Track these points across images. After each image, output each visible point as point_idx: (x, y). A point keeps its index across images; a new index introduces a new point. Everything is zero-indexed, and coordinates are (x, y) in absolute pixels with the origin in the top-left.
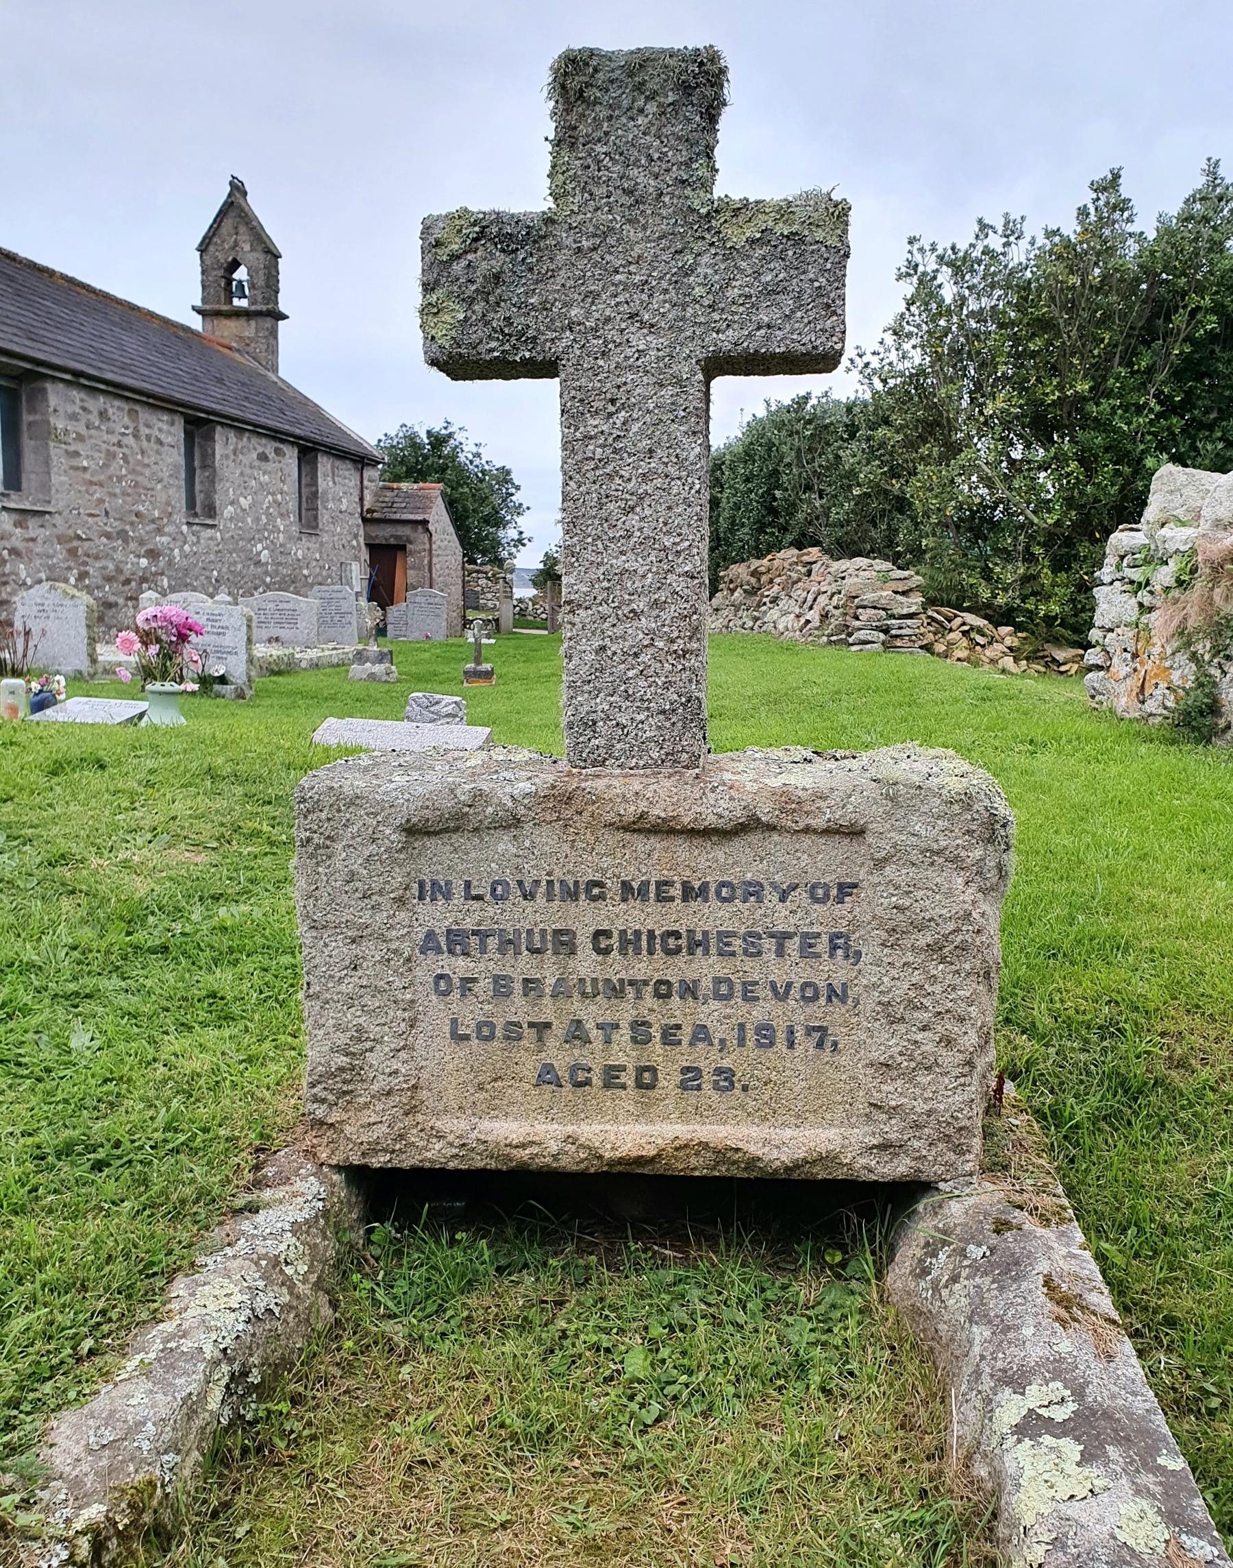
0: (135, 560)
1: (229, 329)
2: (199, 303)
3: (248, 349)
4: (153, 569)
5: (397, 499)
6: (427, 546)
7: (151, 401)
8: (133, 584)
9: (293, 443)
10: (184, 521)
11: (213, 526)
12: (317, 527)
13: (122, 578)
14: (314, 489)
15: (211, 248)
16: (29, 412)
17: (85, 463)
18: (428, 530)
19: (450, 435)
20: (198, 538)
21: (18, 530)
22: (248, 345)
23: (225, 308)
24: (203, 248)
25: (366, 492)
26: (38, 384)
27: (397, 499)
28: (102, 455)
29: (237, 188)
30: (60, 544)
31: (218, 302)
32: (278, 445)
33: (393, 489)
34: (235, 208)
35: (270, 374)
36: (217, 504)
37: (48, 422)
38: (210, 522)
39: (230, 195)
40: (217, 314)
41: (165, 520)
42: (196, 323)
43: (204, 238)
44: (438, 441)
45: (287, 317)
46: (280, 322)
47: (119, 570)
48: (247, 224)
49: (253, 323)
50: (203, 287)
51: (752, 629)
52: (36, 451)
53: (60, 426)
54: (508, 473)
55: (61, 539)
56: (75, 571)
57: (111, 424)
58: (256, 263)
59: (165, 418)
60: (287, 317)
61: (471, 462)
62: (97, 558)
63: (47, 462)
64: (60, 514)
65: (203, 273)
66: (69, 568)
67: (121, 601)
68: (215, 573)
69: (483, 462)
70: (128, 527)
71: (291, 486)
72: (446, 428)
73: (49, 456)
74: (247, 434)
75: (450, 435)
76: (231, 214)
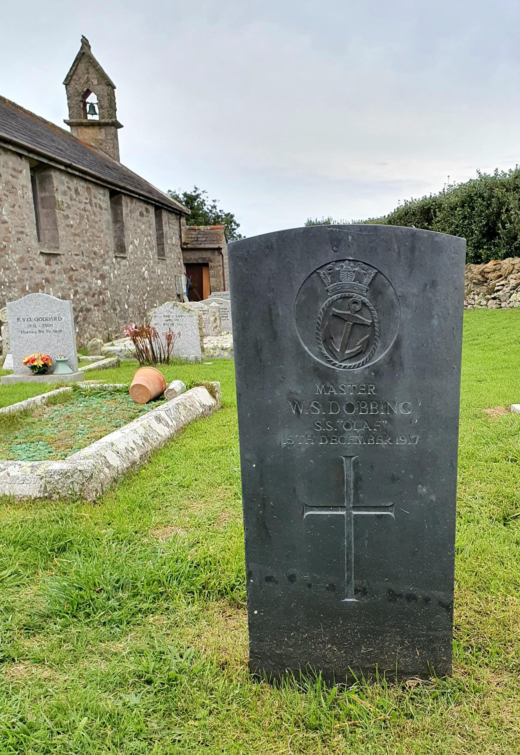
0: (96, 281)
1: (87, 135)
2: (67, 118)
3: (101, 147)
4: (103, 286)
5: (199, 236)
6: (221, 263)
7: (98, 181)
8: (96, 296)
9: (152, 204)
10: (114, 255)
11: (125, 258)
12: (164, 255)
13: (91, 293)
14: (161, 232)
15: (72, 82)
16: (42, 192)
17: (72, 223)
18: (221, 253)
19: (198, 196)
20: (120, 265)
21: (47, 267)
22: (101, 144)
23: (85, 121)
24: (67, 82)
25: (182, 232)
26: (48, 173)
27: (199, 236)
28: (78, 217)
29: (85, 42)
30: (65, 274)
31: (80, 117)
32: (146, 206)
33: (195, 230)
34: (85, 56)
35: (117, 162)
36: (126, 244)
37: (54, 197)
38: (122, 255)
39: (82, 48)
40: (80, 125)
41: (106, 256)
42: (67, 128)
43: (68, 76)
44: (190, 199)
45: (122, 126)
46: (118, 130)
47: (90, 288)
48: (94, 67)
49: (103, 130)
50: (69, 107)
51: (486, 305)
52: (47, 215)
53: (60, 200)
54: (232, 216)
55: (66, 271)
56: (72, 290)
57: (80, 197)
58: (102, 92)
59: (102, 192)
60: (122, 126)
61: (211, 211)
62: (81, 281)
63: (55, 223)
64: (64, 255)
65: (68, 98)
66: (70, 289)
67: (92, 307)
68: (128, 286)
69: (218, 211)
70: (91, 261)
71: (153, 231)
72: (195, 192)
73: (56, 218)
74: (135, 200)
75: (198, 196)
76: (84, 61)
